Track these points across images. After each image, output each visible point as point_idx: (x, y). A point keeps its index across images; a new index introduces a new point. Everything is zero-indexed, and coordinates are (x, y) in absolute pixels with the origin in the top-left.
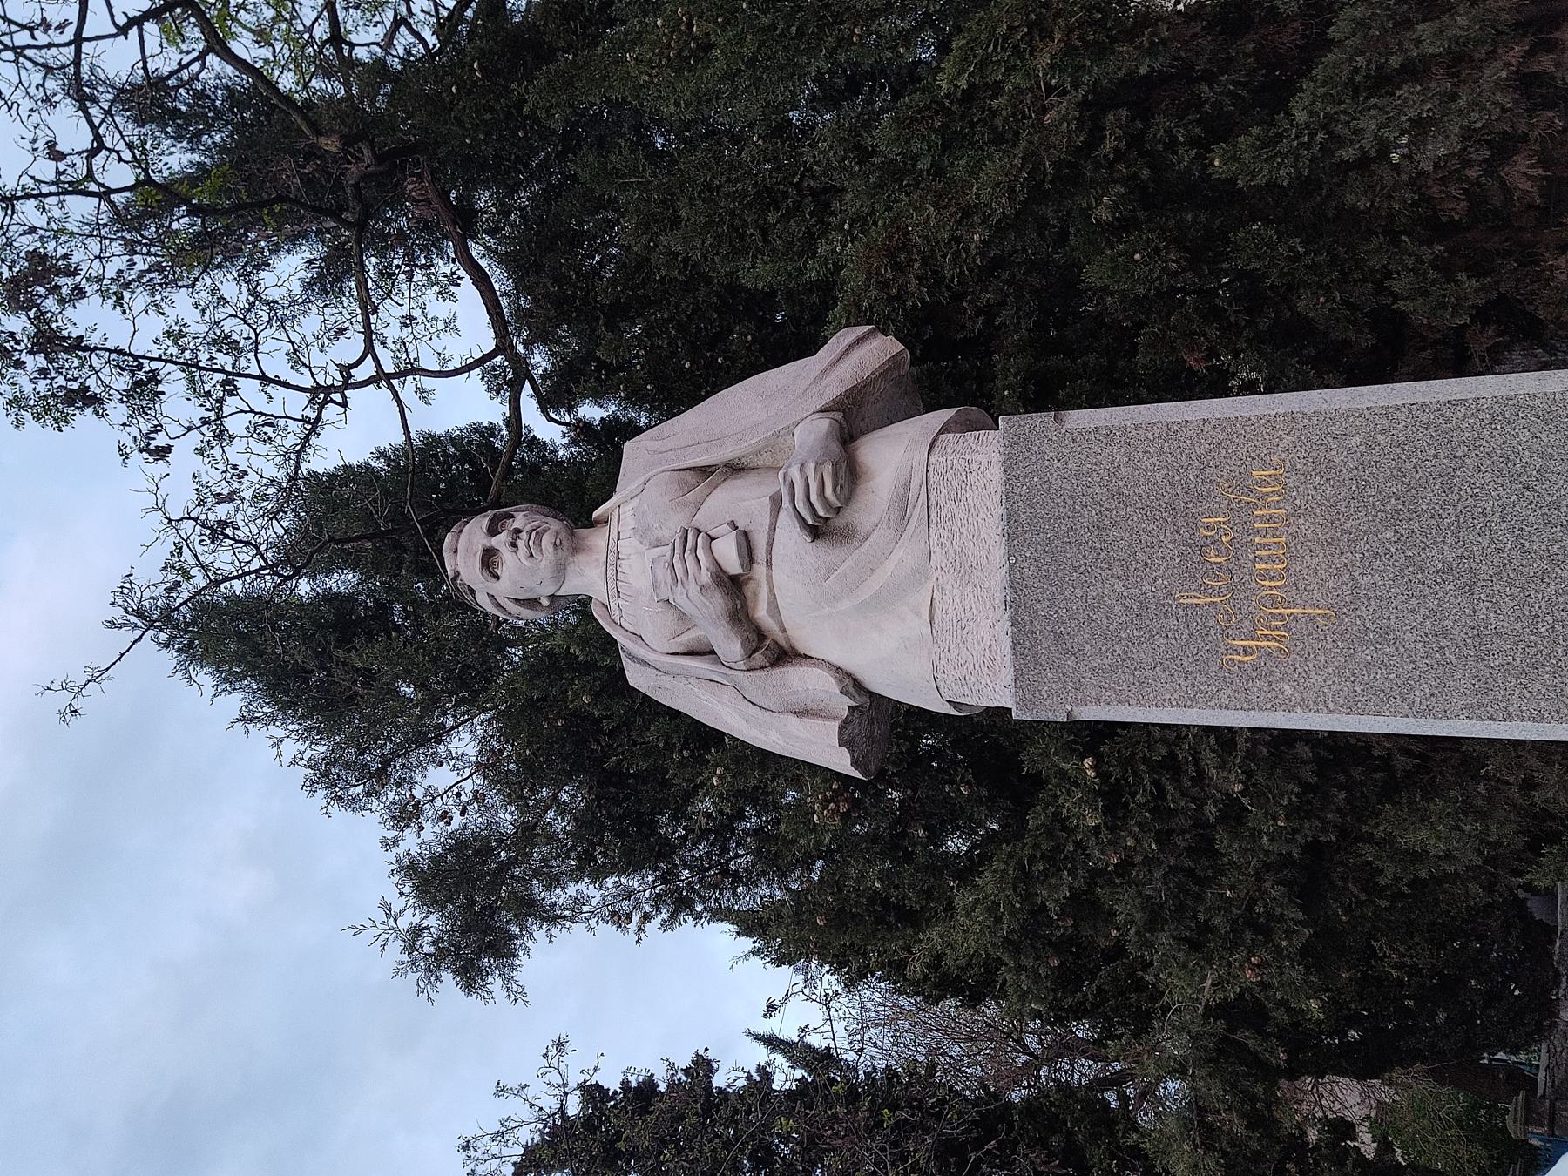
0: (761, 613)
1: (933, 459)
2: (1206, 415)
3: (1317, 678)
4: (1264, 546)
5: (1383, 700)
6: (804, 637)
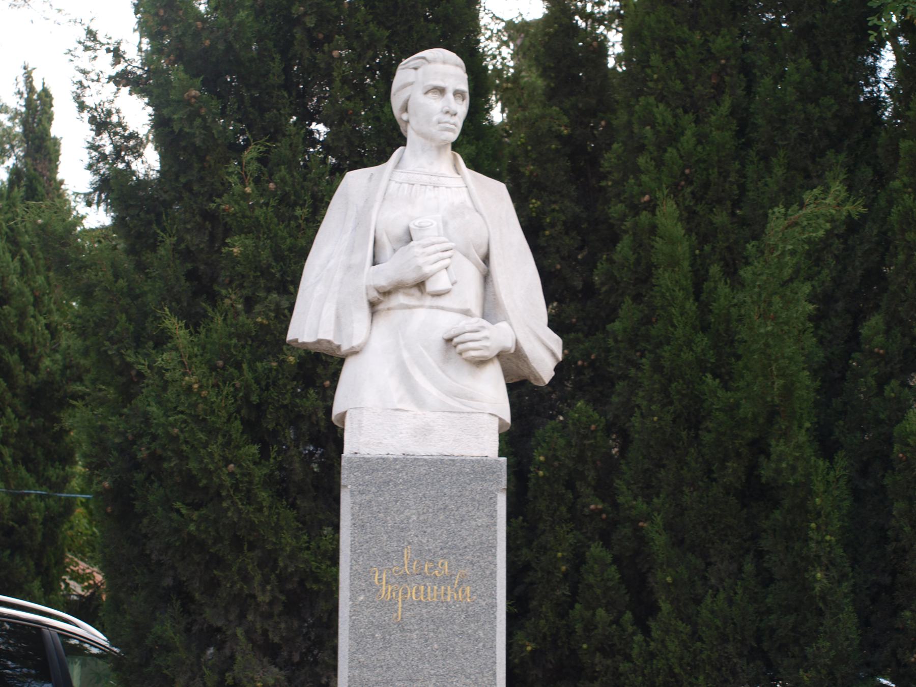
0: (400, 299)
1: (486, 417)
2: (498, 566)
3: (367, 612)
4: (432, 590)
5: (357, 640)
6: (383, 323)
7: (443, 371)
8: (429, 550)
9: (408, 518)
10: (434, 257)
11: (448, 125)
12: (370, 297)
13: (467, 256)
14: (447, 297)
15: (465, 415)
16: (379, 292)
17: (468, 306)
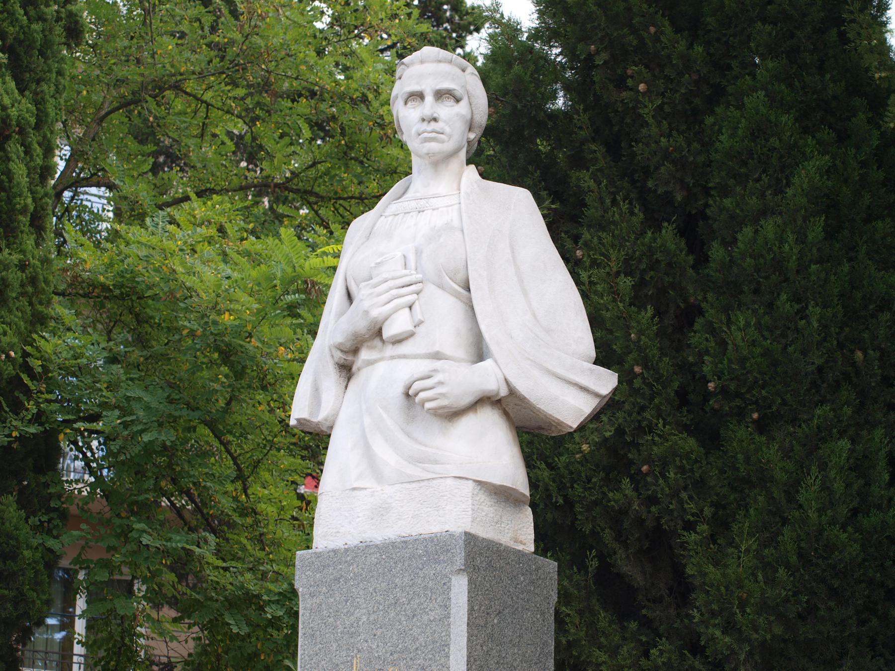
0: (365, 355)
1: (449, 482)
7: (408, 435)
8: (379, 657)
9: (358, 620)
11: (425, 135)
12: (336, 360)
13: (441, 286)
14: (411, 342)
15: (425, 483)
16: (342, 351)
17: (437, 348)
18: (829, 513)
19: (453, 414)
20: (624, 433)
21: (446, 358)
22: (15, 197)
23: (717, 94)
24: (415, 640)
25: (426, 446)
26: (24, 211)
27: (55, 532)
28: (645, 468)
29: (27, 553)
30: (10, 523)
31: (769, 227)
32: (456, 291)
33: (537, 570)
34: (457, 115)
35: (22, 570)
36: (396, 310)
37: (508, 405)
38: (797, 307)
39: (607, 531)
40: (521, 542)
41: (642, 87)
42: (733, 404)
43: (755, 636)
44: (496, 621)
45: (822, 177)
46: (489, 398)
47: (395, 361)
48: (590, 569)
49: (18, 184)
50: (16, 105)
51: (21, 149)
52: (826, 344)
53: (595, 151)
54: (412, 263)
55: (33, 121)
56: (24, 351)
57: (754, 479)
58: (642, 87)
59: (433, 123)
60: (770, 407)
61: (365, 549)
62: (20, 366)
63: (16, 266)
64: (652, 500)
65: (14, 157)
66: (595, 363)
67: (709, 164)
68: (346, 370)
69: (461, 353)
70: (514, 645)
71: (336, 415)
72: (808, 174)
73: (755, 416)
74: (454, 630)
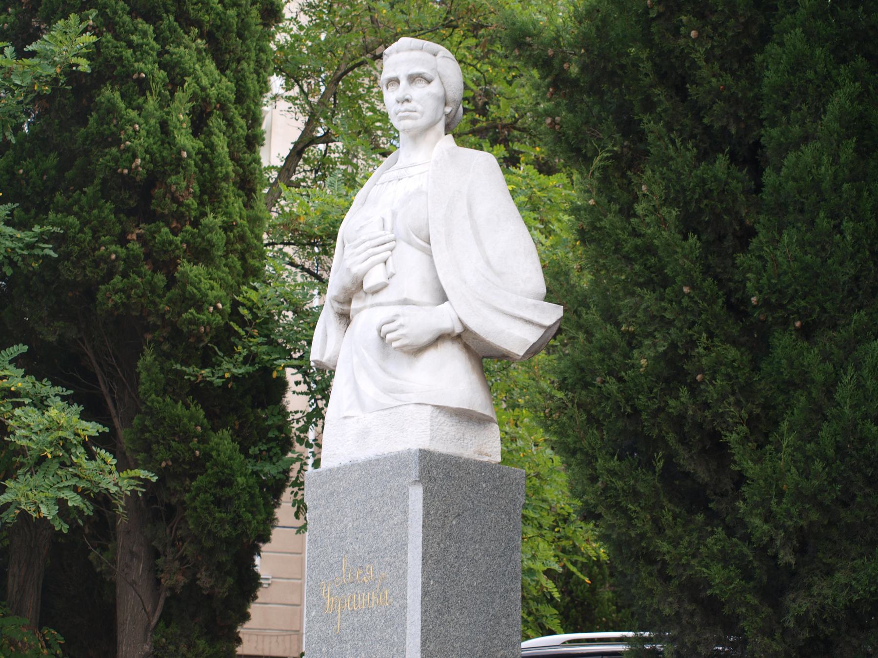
0: (355, 305)
7: (384, 370)
8: (360, 556)
9: (346, 526)
10: (364, 255)
11: (400, 114)
13: (410, 243)
14: (385, 292)
16: (339, 302)
17: (405, 296)
18: (863, 408)
19: (418, 351)
20: (676, 347)
21: (414, 304)
22: (217, 167)
23: (765, 36)
24: (384, 541)
25: (396, 378)
26: (226, 178)
27: (275, 459)
28: (699, 377)
29: (241, 480)
30: (225, 454)
31: (808, 152)
32: (421, 246)
33: (502, 477)
34: (428, 94)
35: (237, 495)
36: (372, 266)
37: (464, 339)
38: (833, 222)
39: (671, 435)
40: (486, 455)
41: (693, 34)
42: (777, 315)
43: (789, 523)
44: (454, 522)
45: (852, 102)
46: (449, 335)
47: (374, 309)
48: (657, 469)
49: (220, 154)
50: (216, 84)
51: (223, 123)
52: (860, 255)
53: (659, 95)
54: (388, 225)
55: (232, 97)
56: (234, 300)
57: (797, 381)
58: (693, 34)
59: (406, 104)
60: (811, 316)
61: (353, 466)
62: (230, 315)
63: (220, 227)
64: (706, 406)
65: (217, 131)
66: (545, 300)
67: (758, 98)
68: (345, 318)
69: (426, 298)
70: (475, 542)
71: (337, 356)
72: (839, 101)
73: (798, 324)
74: (411, 531)
